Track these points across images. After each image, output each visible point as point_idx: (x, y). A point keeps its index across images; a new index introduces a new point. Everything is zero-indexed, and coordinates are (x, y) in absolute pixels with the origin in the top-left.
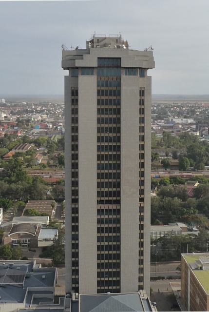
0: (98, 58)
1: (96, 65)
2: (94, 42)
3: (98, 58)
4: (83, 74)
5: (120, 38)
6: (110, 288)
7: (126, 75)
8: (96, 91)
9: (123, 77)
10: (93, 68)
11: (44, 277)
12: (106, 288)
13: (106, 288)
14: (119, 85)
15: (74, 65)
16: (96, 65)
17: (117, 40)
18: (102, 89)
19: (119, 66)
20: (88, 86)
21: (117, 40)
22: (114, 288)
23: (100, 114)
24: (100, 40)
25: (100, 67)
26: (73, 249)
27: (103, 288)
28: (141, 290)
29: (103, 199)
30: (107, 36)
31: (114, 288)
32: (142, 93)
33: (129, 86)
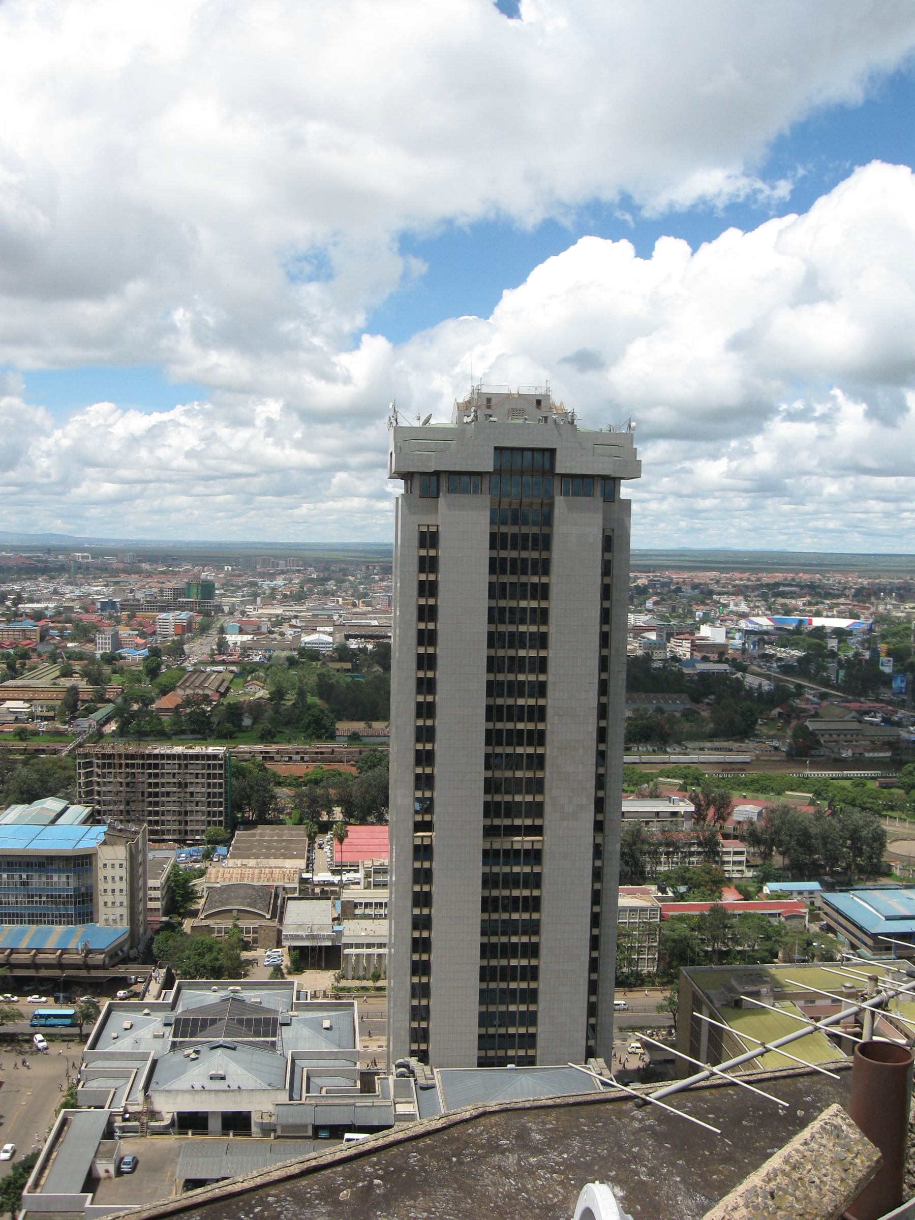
0: (496, 448)
1: (488, 465)
2: (483, 405)
3: (496, 448)
4: (451, 490)
5: (547, 396)
6: (511, 1053)
7: (566, 494)
8: (585, 1005)
9: (560, 502)
10: (480, 474)
11: (326, 1024)
12: (501, 1053)
13: (501, 1053)
14: (547, 520)
15: (426, 482)
16: (488, 465)
17: (539, 402)
18: (511, 581)
19: (548, 472)
20: (467, 530)
21: (539, 402)
22: (521, 1052)
23: (494, 598)
24: (493, 402)
25: (498, 472)
26: (538, 921)
27: (491, 1053)
28: (592, 1060)
29: (497, 822)
30: (514, 391)
31: (521, 1052)
32: (608, 543)
33: (574, 530)
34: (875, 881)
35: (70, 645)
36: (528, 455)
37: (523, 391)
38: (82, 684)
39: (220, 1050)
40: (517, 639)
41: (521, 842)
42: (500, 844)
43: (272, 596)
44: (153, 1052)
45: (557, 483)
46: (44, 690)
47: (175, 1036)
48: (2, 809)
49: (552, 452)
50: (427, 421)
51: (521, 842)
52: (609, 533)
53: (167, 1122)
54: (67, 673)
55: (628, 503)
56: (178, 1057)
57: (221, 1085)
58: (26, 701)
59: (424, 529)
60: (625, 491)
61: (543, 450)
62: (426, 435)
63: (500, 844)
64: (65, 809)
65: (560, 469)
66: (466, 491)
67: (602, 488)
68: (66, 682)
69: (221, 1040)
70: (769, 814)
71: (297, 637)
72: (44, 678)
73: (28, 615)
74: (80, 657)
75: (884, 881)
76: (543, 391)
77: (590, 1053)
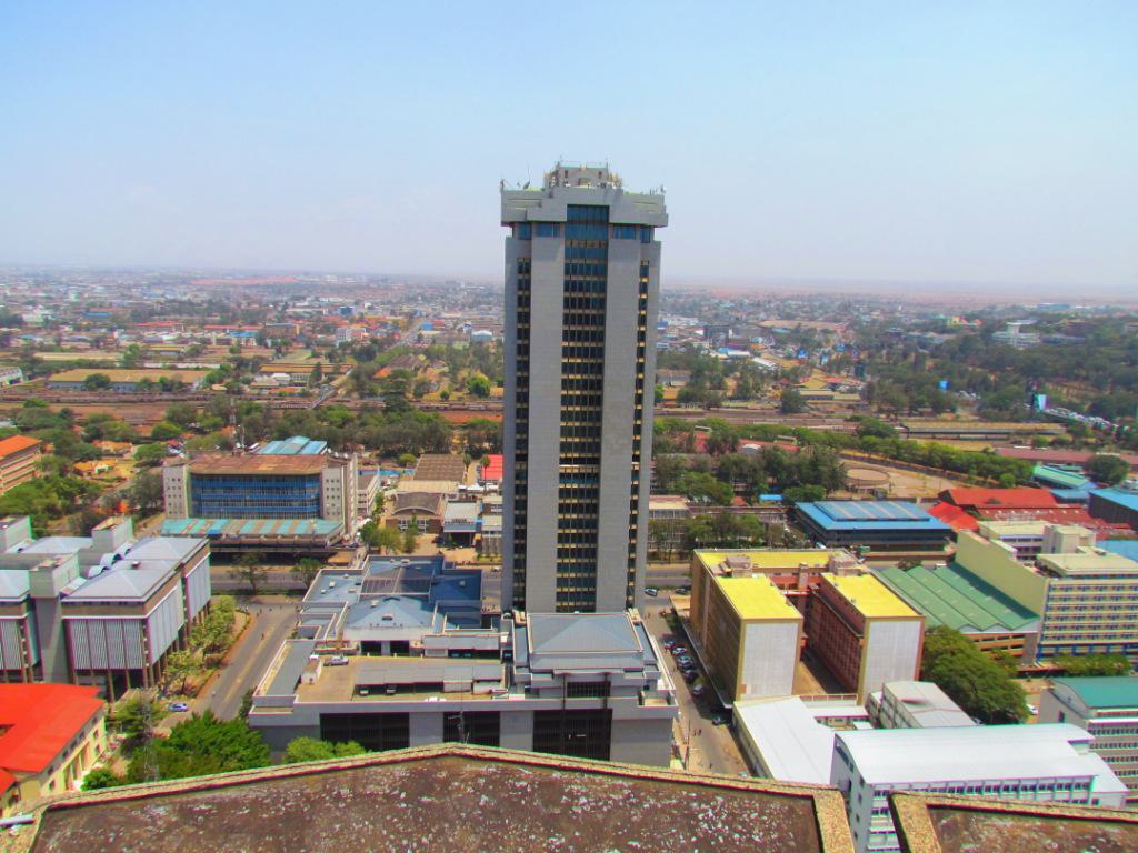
0: (569, 206)
1: (564, 218)
3: (569, 206)
5: (606, 169)
15: (525, 231)
17: (600, 173)
21: (600, 173)
22: (585, 604)
25: (570, 222)
27: (565, 604)
30: (584, 166)
34: (284, 654)
35: (319, 336)
36: (590, 210)
37: (590, 166)
38: (324, 361)
39: (392, 601)
40: (583, 335)
41: (574, 468)
42: (588, 469)
43: (456, 304)
44: (347, 602)
45: (610, 229)
46: (301, 366)
47: (363, 591)
48: (1132, 319)
49: (607, 208)
50: (526, 187)
51: (574, 468)
52: (645, 264)
53: (353, 647)
54: (316, 355)
55: (659, 244)
56: (364, 605)
57: (389, 623)
58: (287, 373)
59: (521, 261)
60: (658, 235)
61: (601, 207)
62: (524, 195)
63: (588, 469)
64: (307, 444)
65: (613, 219)
66: (548, 235)
67: (642, 232)
68: (314, 361)
69: (393, 594)
70: (763, 452)
71: (469, 332)
72: (302, 357)
73: (290, 317)
74: (325, 345)
75: (839, 494)
76: (603, 166)
77: (629, 605)
